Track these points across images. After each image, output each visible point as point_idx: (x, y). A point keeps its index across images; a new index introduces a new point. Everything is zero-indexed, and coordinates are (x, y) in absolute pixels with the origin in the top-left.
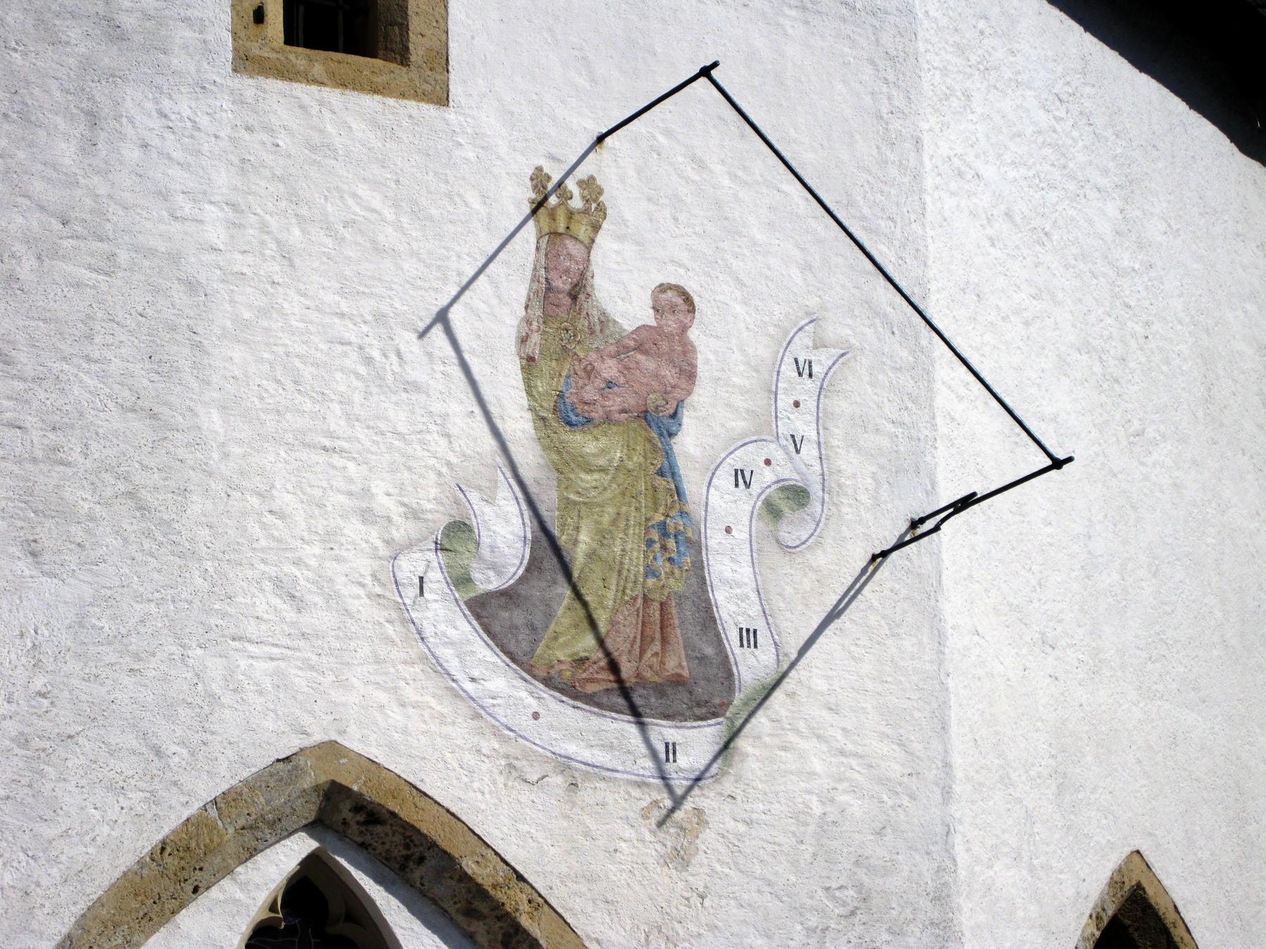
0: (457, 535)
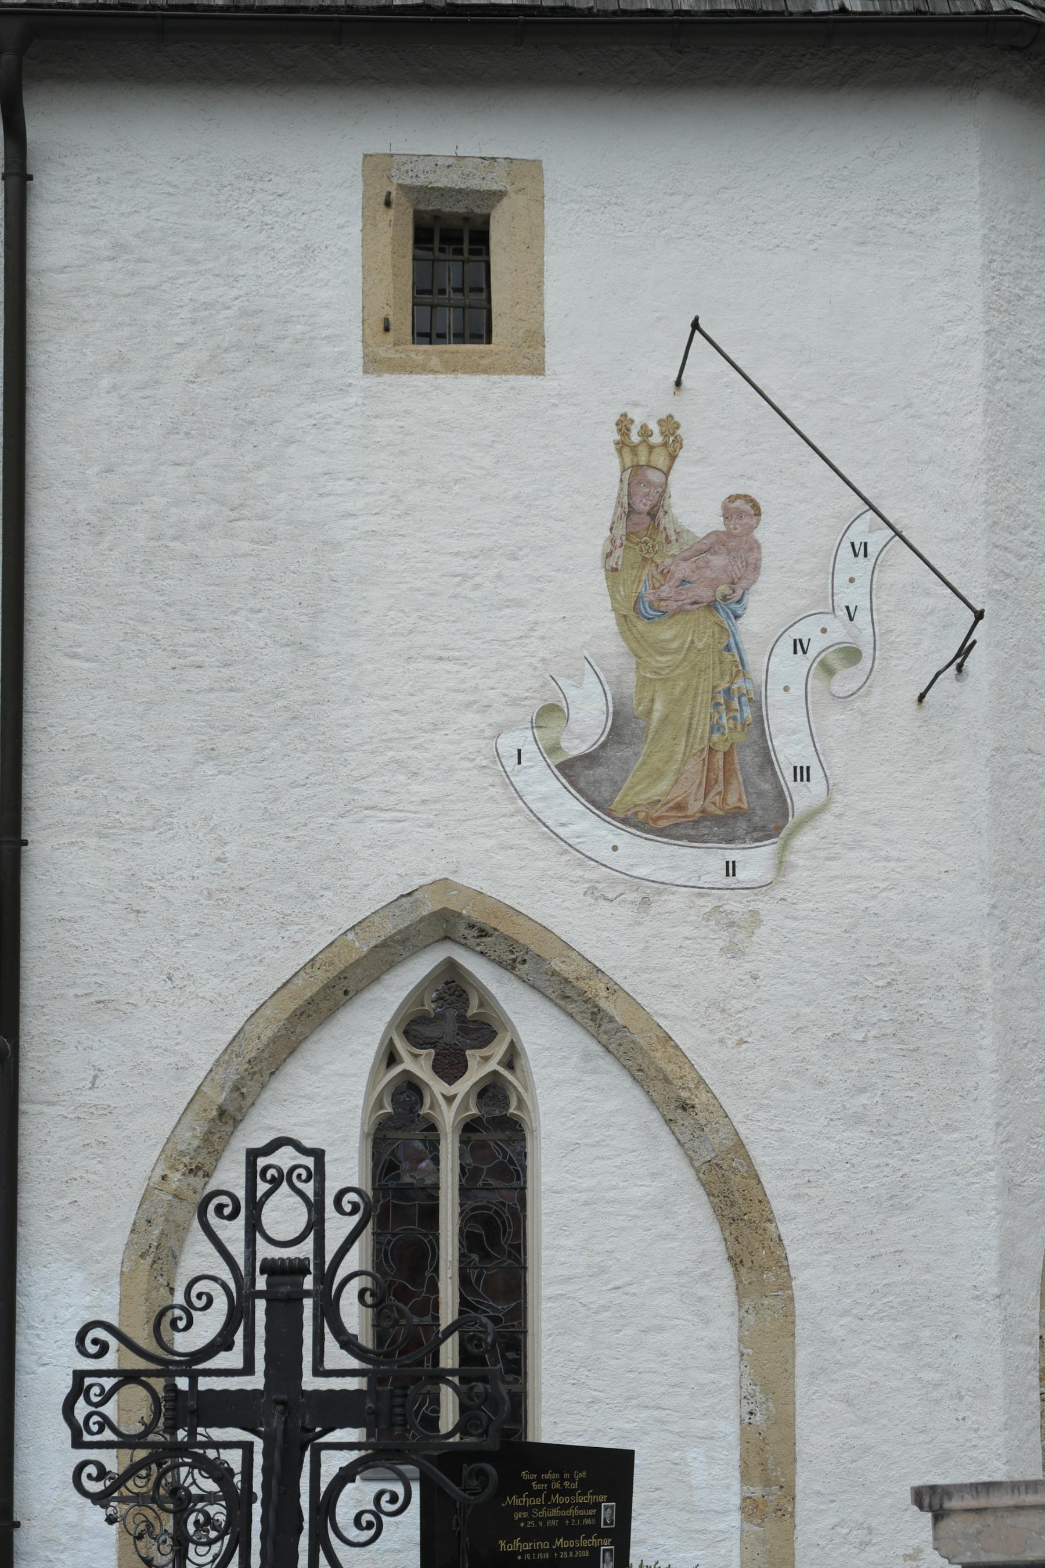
0: (551, 712)
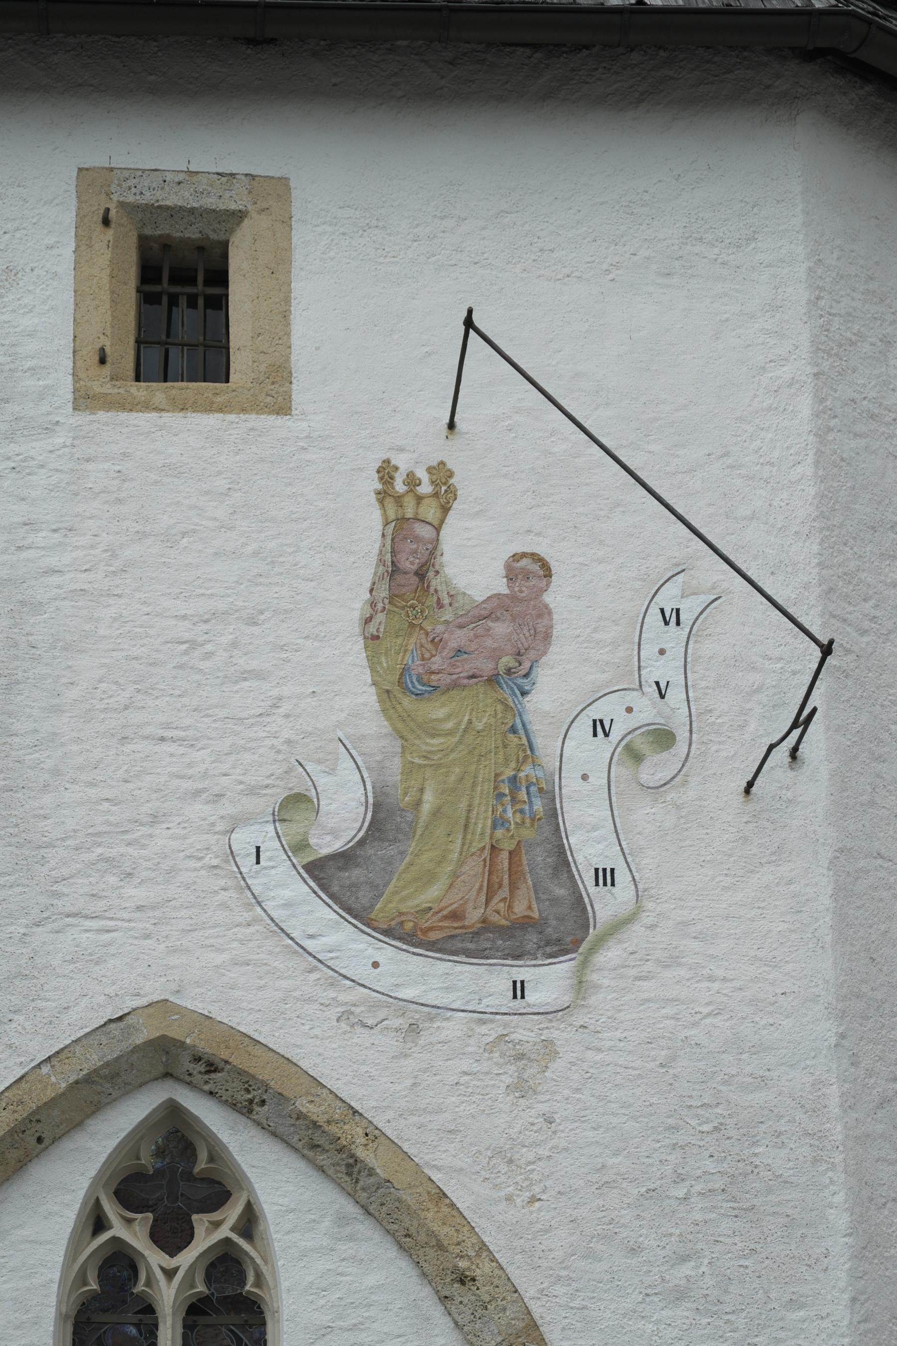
0: (297, 803)
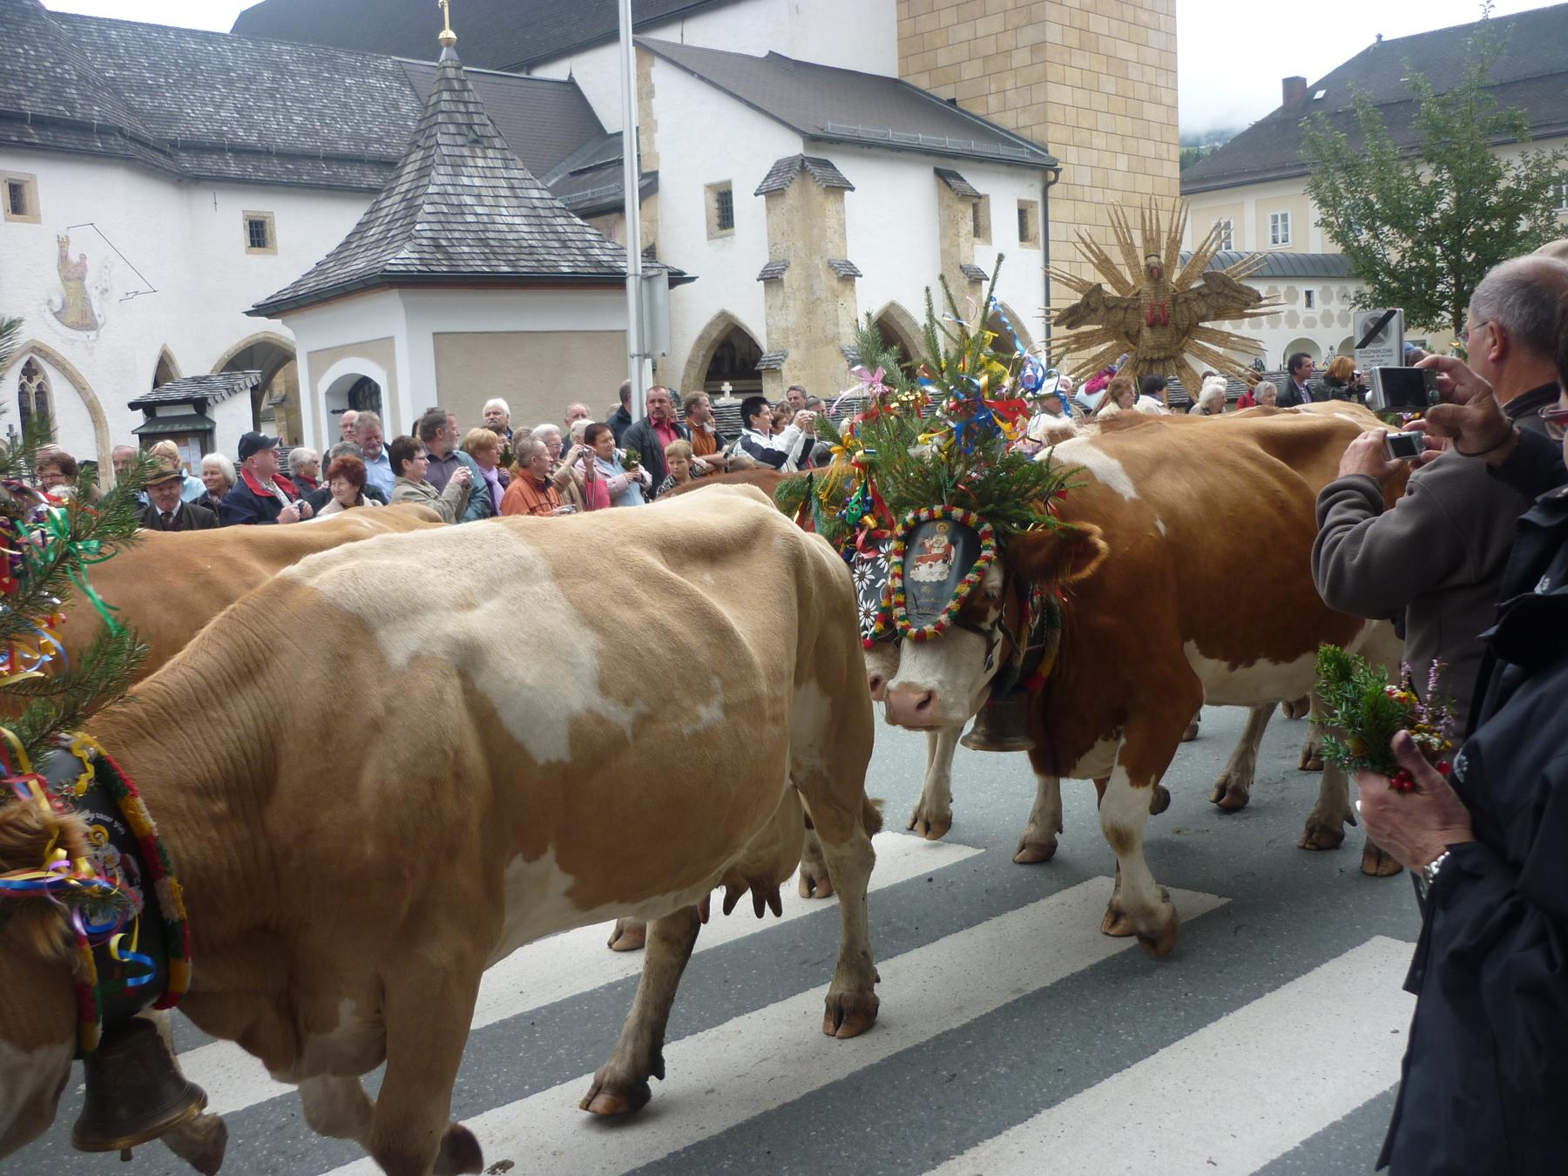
0: (50, 302)
